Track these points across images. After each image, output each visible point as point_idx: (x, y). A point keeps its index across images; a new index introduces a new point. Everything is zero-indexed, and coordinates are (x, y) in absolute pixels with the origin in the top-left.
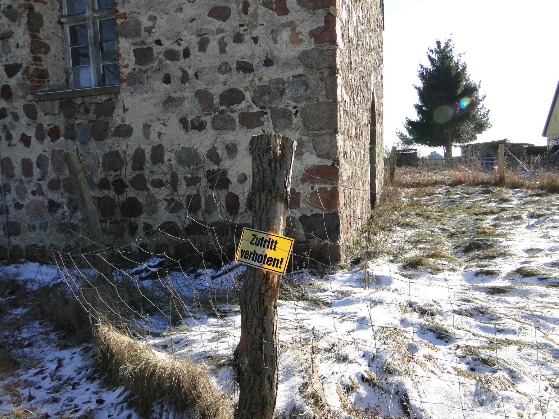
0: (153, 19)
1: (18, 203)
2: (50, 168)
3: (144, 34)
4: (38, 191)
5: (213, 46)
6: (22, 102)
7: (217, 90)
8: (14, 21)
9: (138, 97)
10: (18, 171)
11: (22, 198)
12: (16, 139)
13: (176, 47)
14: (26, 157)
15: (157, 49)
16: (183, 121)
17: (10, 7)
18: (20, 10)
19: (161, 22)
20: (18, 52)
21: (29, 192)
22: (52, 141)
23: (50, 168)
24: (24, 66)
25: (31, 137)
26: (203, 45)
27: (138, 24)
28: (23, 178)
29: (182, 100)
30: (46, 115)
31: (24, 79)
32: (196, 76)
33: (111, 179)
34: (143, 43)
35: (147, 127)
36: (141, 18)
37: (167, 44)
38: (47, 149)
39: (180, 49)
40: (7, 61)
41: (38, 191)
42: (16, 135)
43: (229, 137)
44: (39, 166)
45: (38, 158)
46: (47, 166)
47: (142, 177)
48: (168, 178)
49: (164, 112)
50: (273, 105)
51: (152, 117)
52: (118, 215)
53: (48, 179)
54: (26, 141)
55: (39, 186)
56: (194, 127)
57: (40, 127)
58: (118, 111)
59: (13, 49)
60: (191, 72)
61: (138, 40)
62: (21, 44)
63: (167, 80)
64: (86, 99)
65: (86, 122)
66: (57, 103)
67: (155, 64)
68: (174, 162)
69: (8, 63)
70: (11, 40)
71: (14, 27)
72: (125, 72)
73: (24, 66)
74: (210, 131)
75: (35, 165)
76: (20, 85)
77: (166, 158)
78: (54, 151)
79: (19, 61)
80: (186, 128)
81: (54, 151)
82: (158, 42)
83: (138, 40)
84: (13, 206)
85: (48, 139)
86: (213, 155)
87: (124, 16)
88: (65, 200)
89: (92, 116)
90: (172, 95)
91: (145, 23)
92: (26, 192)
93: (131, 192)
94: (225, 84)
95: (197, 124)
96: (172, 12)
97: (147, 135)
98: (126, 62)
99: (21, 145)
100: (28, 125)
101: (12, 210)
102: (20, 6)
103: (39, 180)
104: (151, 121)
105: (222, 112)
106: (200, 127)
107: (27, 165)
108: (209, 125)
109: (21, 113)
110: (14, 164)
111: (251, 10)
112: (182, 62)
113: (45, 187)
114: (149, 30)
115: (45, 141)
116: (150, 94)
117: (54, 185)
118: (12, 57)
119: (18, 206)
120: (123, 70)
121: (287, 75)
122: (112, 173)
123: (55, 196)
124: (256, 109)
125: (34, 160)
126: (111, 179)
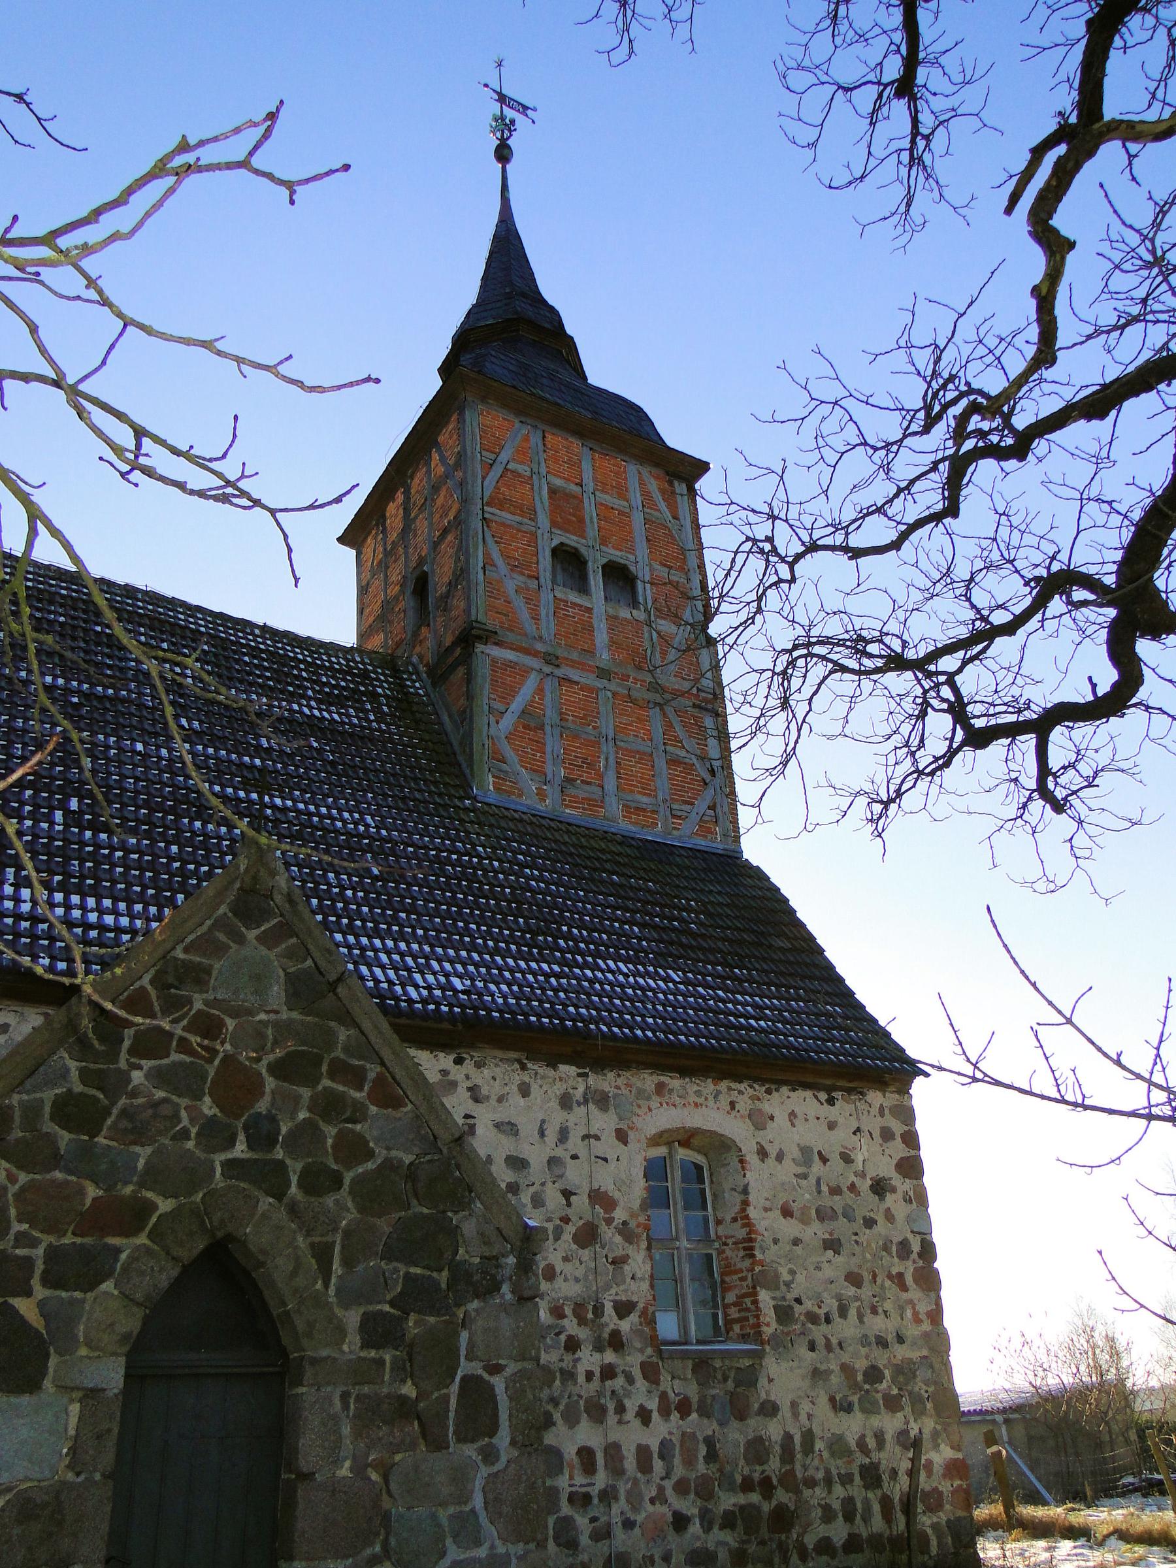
0: (792, 1272)
1: (628, 1519)
2: (677, 1461)
3: (783, 1288)
4: (659, 1498)
5: (852, 1313)
6: (640, 1358)
7: (861, 1365)
8: (631, 1243)
9: (784, 1365)
10: (630, 1463)
11: (636, 1509)
12: (630, 1415)
13: (816, 1309)
14: (644, 1442)
15: (798, 1309)
16: (832, 1400)
17: (625, 1223)
18: (640, 1230)
19: (800, 1278)
20: (633, 1286)
21: (647, 1499)
22: (682, 1418)
23: (677, 1461)
24: (641, 1305)
25: (651, 1411)
26: (843, 1311)
27: (777, 1276)
28: (639, 1475)
29: (828, 1372)
30: (673, 1378)
31: (641, 1324)
32: (840, 1344)
33: (756, 1476)
34: (784, 1298)
35: (794, 1405)
36: (781, 1269)
37: (809, 1305)
38: (675, 1431)
39: (821, 1312)
40: (617, 1294)
41: (659, 1498)
42: (631, 1406)
43: (875, 1422)
44: (662, 1456)
45: (662, 1443)
46: (674, 1456)
47: (792, 1472)
48: (820, 1475)
49: (813, 1386)
50: (909, 1388)
51: (801, 1393)
52: (764, 1532)
53: (674, 1479)
54: (644, 1416)
55: (661, 1489)
56: (842, 1409)
57: (663, 1396)
58: (763, 1382)
59: (628, 1280)
60: (834, 1341)
61: (778, 1294)
62: (639, 1275)
63: (812, 1347)
64: (727, 1362)
65: (722, 1394)
66: (690, 1364)
67: (797, 1327)
68: (826, 1454)
69: (618, 1298)
70: (626, 1267)
71: (630, 1250)
72: (768, 1331)
73: (641, 1305)
74: (858, 1415)
75: (655, 1456)
76: (635, 1332)
77: (817, 1447)
78: (684, 1434)
79: (635, 1299)
80: (834, 1407)
81: (684, 1434)
82: (798, 1301)
83: (778, 1294)
84: (620, 1524)
85: (675, 1416)
86: (862, 1444)
87: (761, 1263)
88: (696, 1511)
89: (730, 1385)
90: (818, 1365)
91: (786, 1277)
92: (642, 1499)
93: (782, 1496)
94: (867, 1357)
95: (845, 1404)
96: (811, 1268)
97: (796, 1415)
98: (768, 1319)
99: (636, 1423)
100: (649, 1392)
101: (619, 1532)
102: (638, 1226)
103: (662, 1479)
104: (799, 1397)
105: (867, 1391)
106: (848, 1409)
107: (643, 1453)
108: (856, 1407)
109: (637, 1373)
110: (625, 1453)
111: (879, 1281)
112: (824, 1328)
113: (669, 1492)
114: (788, 1285)
115: (672, 1417)
116: (795, 1364)
117: (682, 1488)
118: (625, 1291)
119: (628, 1524)
120: (764, 1329)
121: (915, 1355)
122: (758, 1468)
123: (679, 1504)
124: (895, 1391)
125: (655, 1448)
126: (756, 1476)
